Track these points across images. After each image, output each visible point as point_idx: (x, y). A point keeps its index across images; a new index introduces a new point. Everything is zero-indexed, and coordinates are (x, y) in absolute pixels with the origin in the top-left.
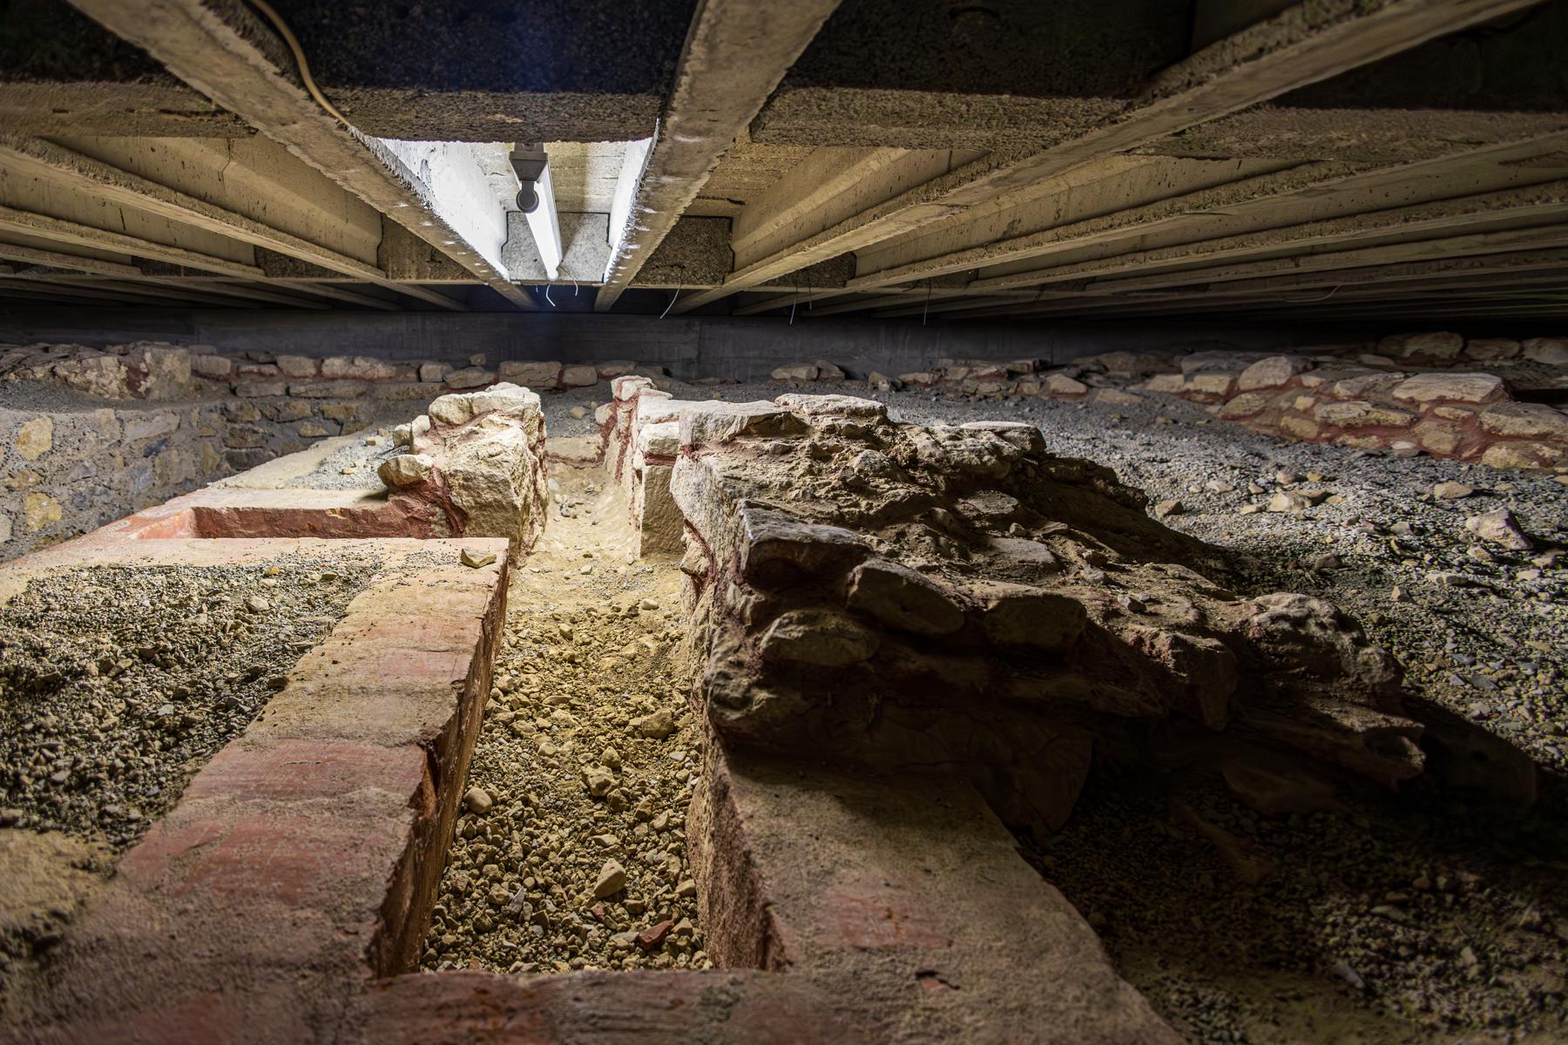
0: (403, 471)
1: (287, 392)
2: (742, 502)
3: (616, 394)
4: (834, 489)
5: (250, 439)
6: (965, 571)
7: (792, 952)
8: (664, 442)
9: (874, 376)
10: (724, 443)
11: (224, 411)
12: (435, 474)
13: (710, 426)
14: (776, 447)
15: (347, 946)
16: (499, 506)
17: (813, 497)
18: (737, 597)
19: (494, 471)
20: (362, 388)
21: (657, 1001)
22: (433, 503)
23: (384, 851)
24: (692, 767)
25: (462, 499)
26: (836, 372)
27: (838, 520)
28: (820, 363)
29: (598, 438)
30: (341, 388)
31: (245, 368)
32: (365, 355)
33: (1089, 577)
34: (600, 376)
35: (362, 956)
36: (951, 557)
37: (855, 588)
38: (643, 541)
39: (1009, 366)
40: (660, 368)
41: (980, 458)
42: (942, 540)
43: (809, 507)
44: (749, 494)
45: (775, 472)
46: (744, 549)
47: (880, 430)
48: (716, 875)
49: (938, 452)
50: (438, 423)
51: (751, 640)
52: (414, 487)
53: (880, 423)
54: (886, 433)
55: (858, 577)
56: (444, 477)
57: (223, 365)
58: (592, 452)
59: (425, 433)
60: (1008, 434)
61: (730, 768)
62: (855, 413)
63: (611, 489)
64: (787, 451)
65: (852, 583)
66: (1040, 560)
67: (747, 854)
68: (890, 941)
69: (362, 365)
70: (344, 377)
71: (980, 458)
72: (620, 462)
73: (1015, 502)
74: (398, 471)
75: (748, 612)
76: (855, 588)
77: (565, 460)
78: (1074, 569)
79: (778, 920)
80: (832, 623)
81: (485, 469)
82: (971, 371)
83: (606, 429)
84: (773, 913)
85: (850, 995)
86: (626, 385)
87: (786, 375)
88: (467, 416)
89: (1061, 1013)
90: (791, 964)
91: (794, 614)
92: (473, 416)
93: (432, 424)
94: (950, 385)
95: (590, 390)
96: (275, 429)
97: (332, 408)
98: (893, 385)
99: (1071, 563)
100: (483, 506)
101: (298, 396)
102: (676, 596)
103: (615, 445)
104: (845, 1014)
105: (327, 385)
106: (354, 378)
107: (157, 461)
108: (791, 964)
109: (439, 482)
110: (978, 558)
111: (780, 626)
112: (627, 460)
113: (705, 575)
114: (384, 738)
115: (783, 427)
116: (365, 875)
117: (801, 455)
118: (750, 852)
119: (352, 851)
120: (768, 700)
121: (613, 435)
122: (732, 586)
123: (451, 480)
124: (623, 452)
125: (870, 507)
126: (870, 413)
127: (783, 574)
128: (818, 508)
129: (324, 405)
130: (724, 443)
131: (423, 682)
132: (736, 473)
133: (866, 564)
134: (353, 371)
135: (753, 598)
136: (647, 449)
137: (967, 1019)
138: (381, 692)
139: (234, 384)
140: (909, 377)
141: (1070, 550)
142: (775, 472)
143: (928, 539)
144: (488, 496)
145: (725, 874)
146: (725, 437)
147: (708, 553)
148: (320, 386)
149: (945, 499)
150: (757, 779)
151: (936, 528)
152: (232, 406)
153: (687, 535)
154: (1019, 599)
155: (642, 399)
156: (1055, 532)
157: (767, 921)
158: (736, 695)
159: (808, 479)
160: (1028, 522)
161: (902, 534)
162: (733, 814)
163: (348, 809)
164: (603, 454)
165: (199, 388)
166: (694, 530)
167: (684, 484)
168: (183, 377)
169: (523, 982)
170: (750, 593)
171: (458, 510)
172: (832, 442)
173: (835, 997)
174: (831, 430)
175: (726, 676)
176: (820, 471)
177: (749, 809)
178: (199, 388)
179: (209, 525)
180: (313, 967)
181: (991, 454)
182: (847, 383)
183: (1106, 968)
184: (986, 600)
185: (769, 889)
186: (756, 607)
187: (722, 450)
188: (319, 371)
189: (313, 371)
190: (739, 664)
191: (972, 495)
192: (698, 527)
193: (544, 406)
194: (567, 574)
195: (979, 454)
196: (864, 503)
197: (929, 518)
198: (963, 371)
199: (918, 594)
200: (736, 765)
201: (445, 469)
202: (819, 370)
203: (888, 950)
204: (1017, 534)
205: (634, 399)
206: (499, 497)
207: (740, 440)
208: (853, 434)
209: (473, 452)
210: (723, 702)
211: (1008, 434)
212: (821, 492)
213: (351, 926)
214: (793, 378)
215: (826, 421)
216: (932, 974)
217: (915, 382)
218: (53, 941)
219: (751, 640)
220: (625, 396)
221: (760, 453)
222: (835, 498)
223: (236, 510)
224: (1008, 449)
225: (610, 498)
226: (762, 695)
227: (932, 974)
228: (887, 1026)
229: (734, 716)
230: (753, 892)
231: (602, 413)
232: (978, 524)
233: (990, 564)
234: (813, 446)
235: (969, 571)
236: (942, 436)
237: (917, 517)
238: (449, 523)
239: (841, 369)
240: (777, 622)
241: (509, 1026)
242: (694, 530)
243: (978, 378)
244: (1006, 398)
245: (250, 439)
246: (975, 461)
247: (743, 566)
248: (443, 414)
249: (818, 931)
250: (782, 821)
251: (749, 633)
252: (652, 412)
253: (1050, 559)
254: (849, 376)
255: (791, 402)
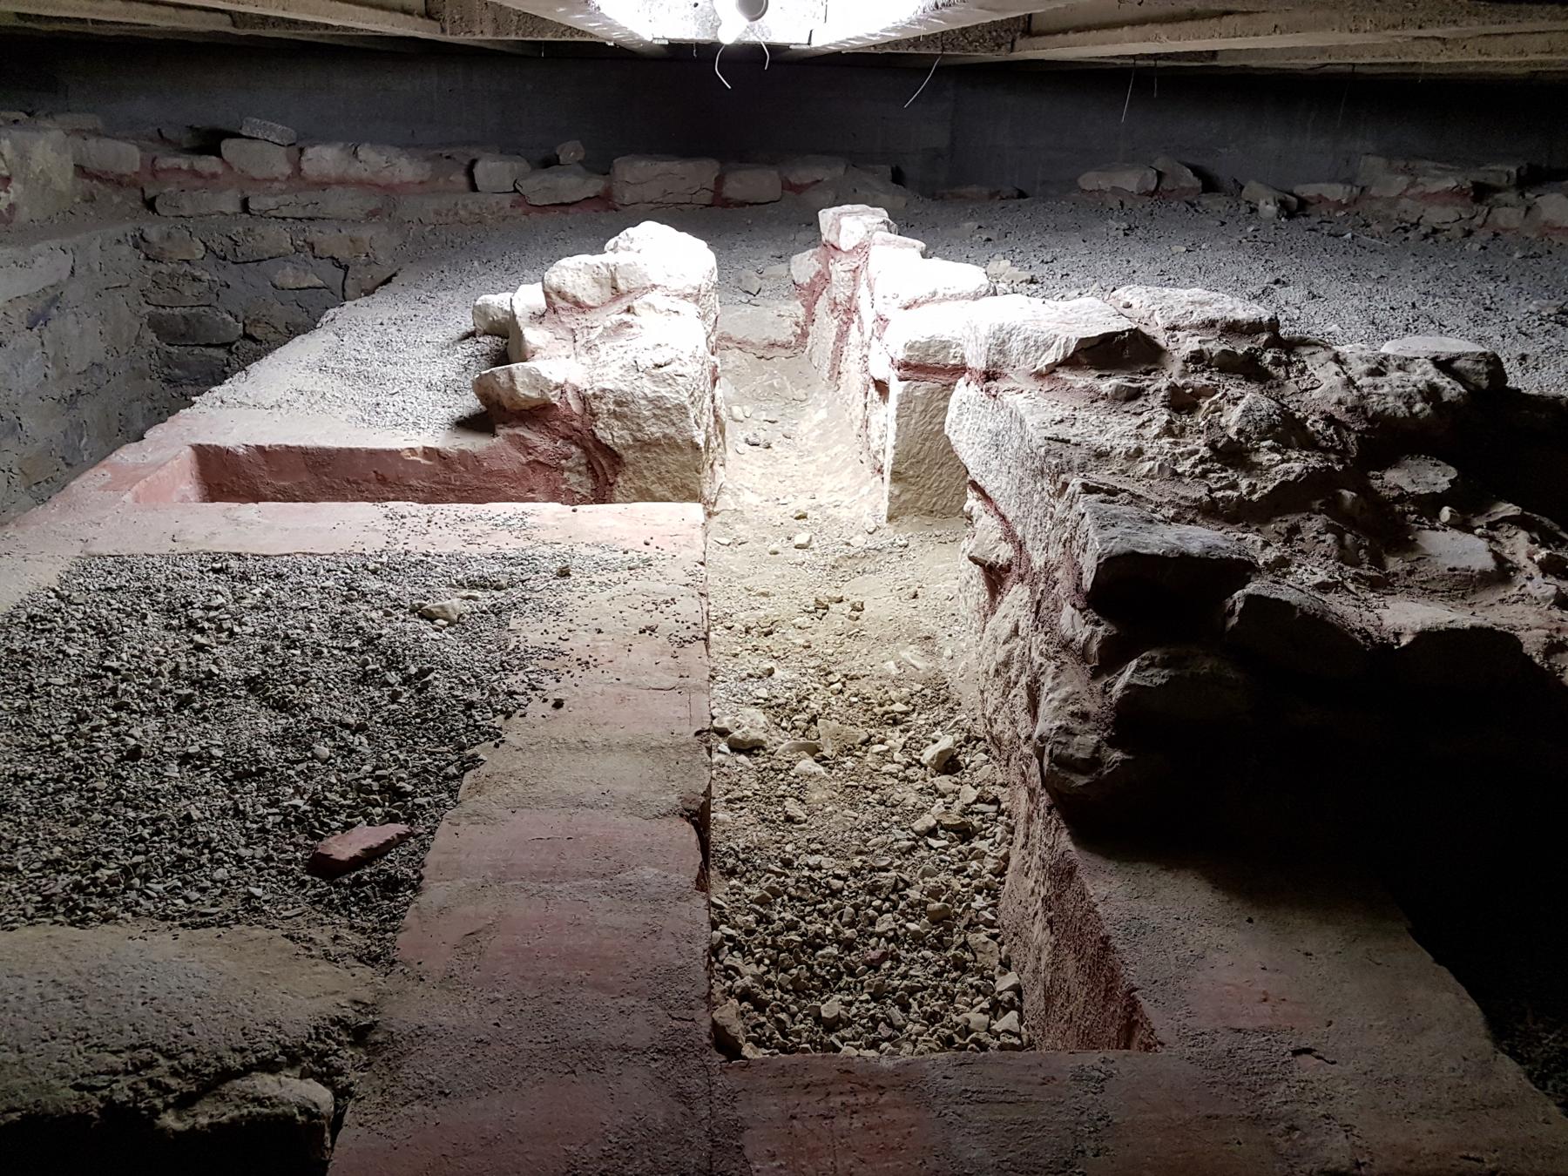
0: (521, 390)
1: (245, 205)
2: (1076, 482)
3: (827, 235)
4: (1202, 461)
5: (189, 291)
6: (1376, 585)
7: (1161, 1035)
8: (928, 345)
9: (1253, 189)
10: (1039, 375)
11: (140, 241)
12: (569, 394)
13: (1016, 345)
14: (1119, 388)
15: (689, 1031)
16: (671, 444)
17: (1175, 473)
18: (1073, 623)
19: (663, 392)
20: (374, 203)
21: (1029, 1078)
22: (567, 438)
23: (691, 939)
24: (1030, 842)
25: (611, 433)
26: (1190, 180)
27: (1210, 511)
28: (1160, 164)
29: (797, 309)
30: (341, 203)
31: (167, 162)
32: (376, 141)
33: (1537, 593)
34: (788, 186)
35: (707, 1041)
36: (1357, 563)
37: (1234, 621)
38: (892, 498)
39: (1477, 176)
40: (887, 170)
41: (1410, 407)
42: (1348, 537)
43: (1169, 490)
44: (1083, 467)
45: (1117, 431)
46: (1089, 564)
47: (1268, 356)
48: (1056, 965)
49: (1351, 397)
50: (560, 303)
51: (1099, 685)
52: (539, 413)
53: (1268, 345)
54: (1277, 362)
55: (1239, 606)
56: (584, 399)
57: (125, 156)
58: (786, 332)
59: (538, 318)
60: (1458, 364)
61: (1076, 844)
62: (1233, 329)
63: (822, 396)
64: (1134, 395)
65: (1232, 612)
66: (1477, 567)
67: (1105, 940)
68: (1267, 1022)
69: (374, 161)
70: (342, 182)
71: (1410, 407)
72: (838, 354)
73: (1453, 473)
74: (513, 390)
75: (1094, 647)
76: (1234, 621)
77: (741, 345)
78: (1520, 579)
79: (1146, 1005)
80: (1206, 666)
81: (648, 387)
82: (1412, 184)
83: (810, 293)
84: (1140, 998)
85: (1225, 1071)
86: (846, 222)
87: (1105, 184)
88: (608, 293)
89: (1435, 1082)
90: (1162, 1044)
91: (1156, 654)
92: (617, 294)
93: (550, 304)
94: (1378, 206)
95: (769, 210)
96: (231, 274)
97: (330, 239)
98: (1283, 205)
99: (1516, 569)
100: (645, 445)
101: (264, 215)
102: (949, 586)
103: (826, 326)
104: (1219, 1087)
105: (315, 195)
106: (360, 183)
107: (47, 336)
108: (1162, 1044)
109: (576, 406)
110: (1394, 564)
111: (1139, 669)
112: (852, 354)
113: (1007, 569)
114: (635, 806)
115: (1127, 354)
116: (680, 963)
117: (1156, 401)
118: (1108, 937)
119: (653, 938)
120: (1123, 761)
121: (822, 305)
122: (1068, 610)
123: (595, 404)
124: (842, 336)
125: (1253, 488)
126: (1254, 328)
127: (1137, 599)
128: (1182, 493)
129: (313, 232)
130: (1039, 375)
131: (659, 735)
132: (1063, 431)
133: (1250, 588)
134: (356, 170)
135: (1101, 628)
136: (901, 356)
137: (1341, 1089)
138: (608, 747)
139: (150, 192)
140: (1309, 191)
141: (1519, 546)
142: (1117, 431)
143: (1330, 538)
144: (654, 430)
145: (1071, 963)
146: (1041, 366)
147: (1009, 535)
148: (303, 199)
149: (1355, 478)
150: (1168, 869)
151: (1341, 521)
152: (153, 234)
153: (972, 502)
154: (1439, 632)
155: (874, 251)
156: (1504, 520)
157: (1133, 1006)
158: (1080, 755)
159: (1166, 442)
160: (1466, 505)
161: (1295, 530)
162: (1083, 895)
163: (628, 892)
164: (805, 335)
165: (90, 199)
166: (985, 496)
167: (968, 421)
168: (64, 179)
169: (886, 1063)
170: (1097, 623)
171: (607, 450)
172: (1200, 380)
173: (1209, 1073)
174: (1197, 357)
175: (1068, 731)
176: (1183, 429)
177: (1103, 890)
178: (90, 199)
179: (225, 476)
180: (660, 1051)
181: (1425, 400)
182: (1206, 200)
183: (1488, 1043)
184: (1397, 635)
185: (1132, 975)
186: (1105, 642)
187: (1032, 386)
188: (298, 169)
189: (288, 170)
190: (1084, 716)
191: (1392, 462)
192: (995, 495)
193: (729, 282)
194: (774, 547)
195: (1409, 400)
196: (1244, 484)
197: (1333, 507)
198: (1402, 180)
199: (1316, 630)
200: (1082, 837)
201: (584, 386)
202: (1160, 175)
203: (1264, 1031)
204: (1452, 524)
205: (862, 249)
206: (671, 431)
207: (1064, 374)
208: (1229, 364)
209: (629, 359)
210: (1065, 763)
211: (1458, 364)
212: (1184, 466)
213: (684, 1013)
214: (1116, 190)
215: (1190, 344)
216: (1308, 1051)
217: (1321, 199)
218: (371, 1027)
219: (1099, 685)
220: (846, 243)
221: (1095, 398)
222: (1204, 474)
223: (260, 449)
224: (1451, 389)
225: (822, 414)
226: (1117, 755)
227: (1308, 1051)
228: (1262, 1095)
229: (1081, 781)
230: (1113, 977)
231: (804, 265)
232: (1398, 508)
233: (1410, 573)
234: (1173, 389)
235: (1382, 584)
236: (1358, 369)
237: (1316, 505)
238: (591, 469)
239: (1197, 171)
240: (1134, 663)
241: (881, 1101)
242: (985, 496)
243: (1425, 196)
244: (1469, 233)
245: (189, 291)
246: (1402, 411)
247: (1087, 583)
248: (569, 290)
249: (1189, 1014)
250: (1142, 902)
251: (1095, 675)
252: (897, 282)
253: (1488, 563)
254: (1210, 185)
255: (1135, 303)
